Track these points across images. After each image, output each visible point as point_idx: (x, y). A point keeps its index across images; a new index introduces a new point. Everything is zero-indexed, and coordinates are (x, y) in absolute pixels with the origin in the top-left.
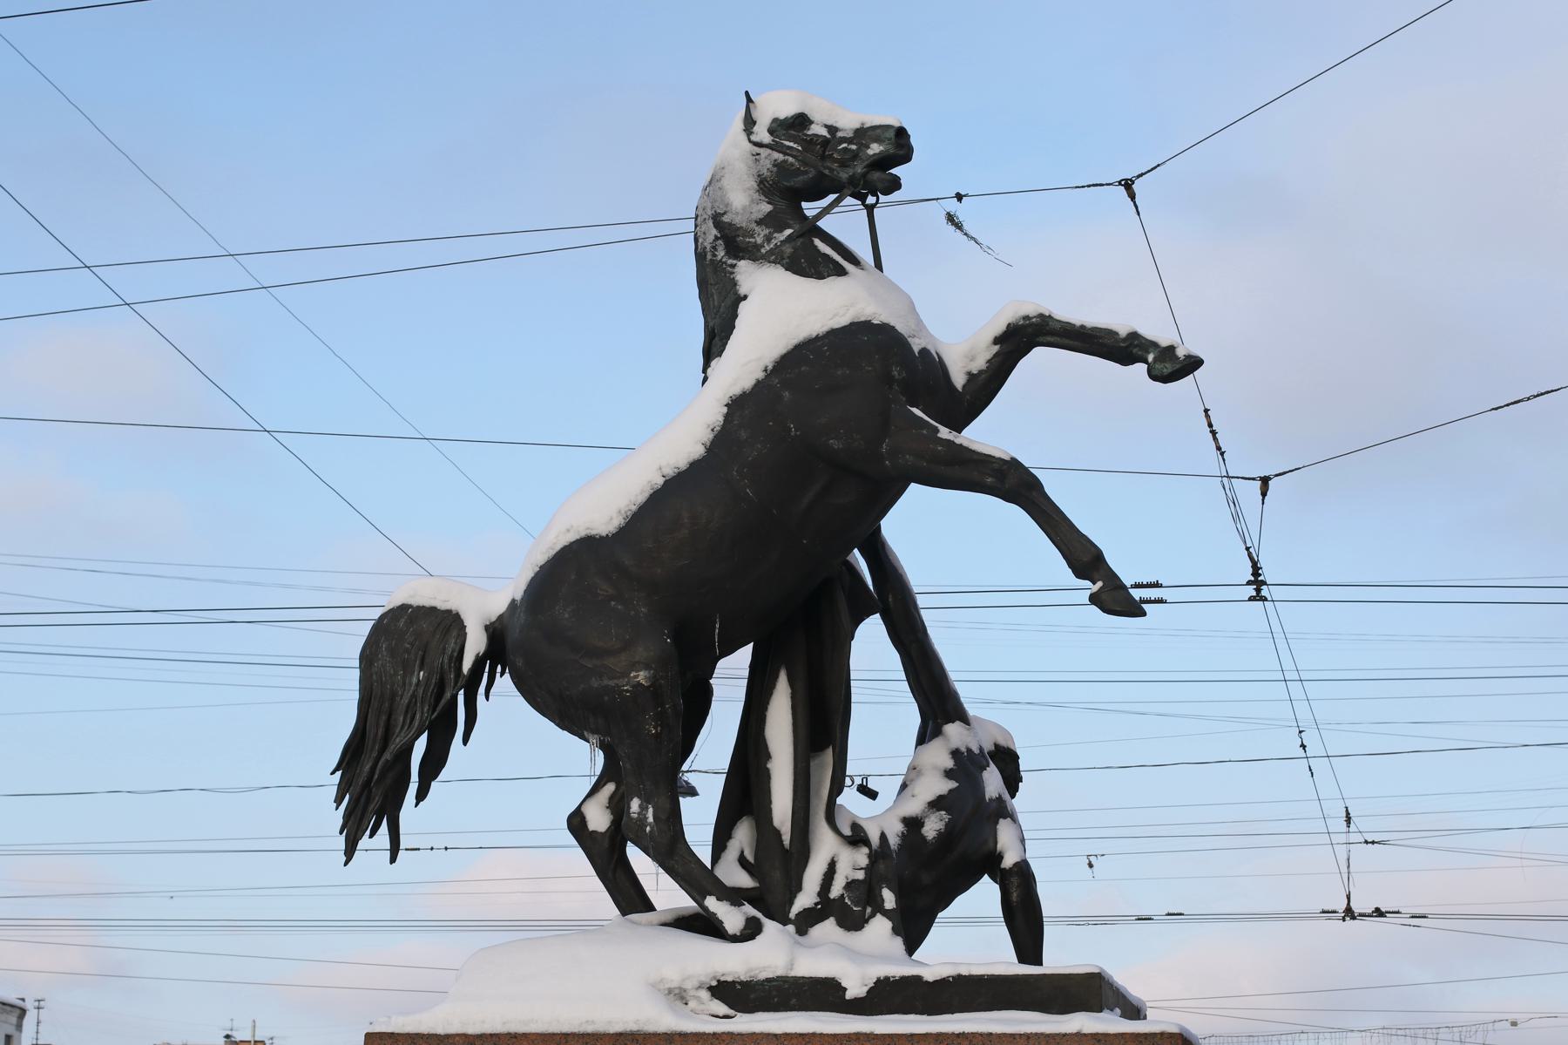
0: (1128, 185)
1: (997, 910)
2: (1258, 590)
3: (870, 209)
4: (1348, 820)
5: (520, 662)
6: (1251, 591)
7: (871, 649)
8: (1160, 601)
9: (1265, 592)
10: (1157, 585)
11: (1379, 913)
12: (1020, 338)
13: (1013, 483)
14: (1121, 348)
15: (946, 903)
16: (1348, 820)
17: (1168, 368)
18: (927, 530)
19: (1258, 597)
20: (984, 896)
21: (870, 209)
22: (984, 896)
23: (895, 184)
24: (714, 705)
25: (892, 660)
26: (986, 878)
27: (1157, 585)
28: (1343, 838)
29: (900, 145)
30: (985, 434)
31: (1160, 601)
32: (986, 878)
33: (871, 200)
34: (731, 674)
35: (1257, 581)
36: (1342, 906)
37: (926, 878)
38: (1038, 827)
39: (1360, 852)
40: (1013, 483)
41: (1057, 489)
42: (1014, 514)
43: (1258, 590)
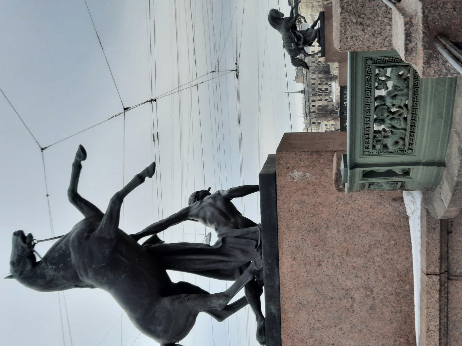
0: (42, 149)
1: (240, 199)
2: (154, 100)
3: (39, 241)
4: (213, 72)
5: (174, 340)
6: (154, 102)
7: (169, 237)
8: (158, 134)
9: (154, 98)
10: (154, 135)
11: (236, 64)
12: (76, 198)
13: (118, 199)
14: (77, 168)
15: (239, 213)
16: (213, 72)
17: (82, 154)
18: (132, 222)
19: (155, 100)
20: (236, 201)
21: (39, 241)
22: (236, 201)
23: (30, 236)
24: (185, 241)
25: (170, 229)
26: (231, 201)
27: (154, 135)
28: (217, 73)
29: (19, 234)
30: (104, 208)
31: (158, 134)
32: (231, 201)
33: (35, 241)
34: (175, 276)
35: (151, 101)
36: (235, 72)
37: (233, 220)
38: (220, 185)
39: (221, 68)
40: (118, 199)
41: (120, 188)
42: (126, 199)
43: (154, 100)
